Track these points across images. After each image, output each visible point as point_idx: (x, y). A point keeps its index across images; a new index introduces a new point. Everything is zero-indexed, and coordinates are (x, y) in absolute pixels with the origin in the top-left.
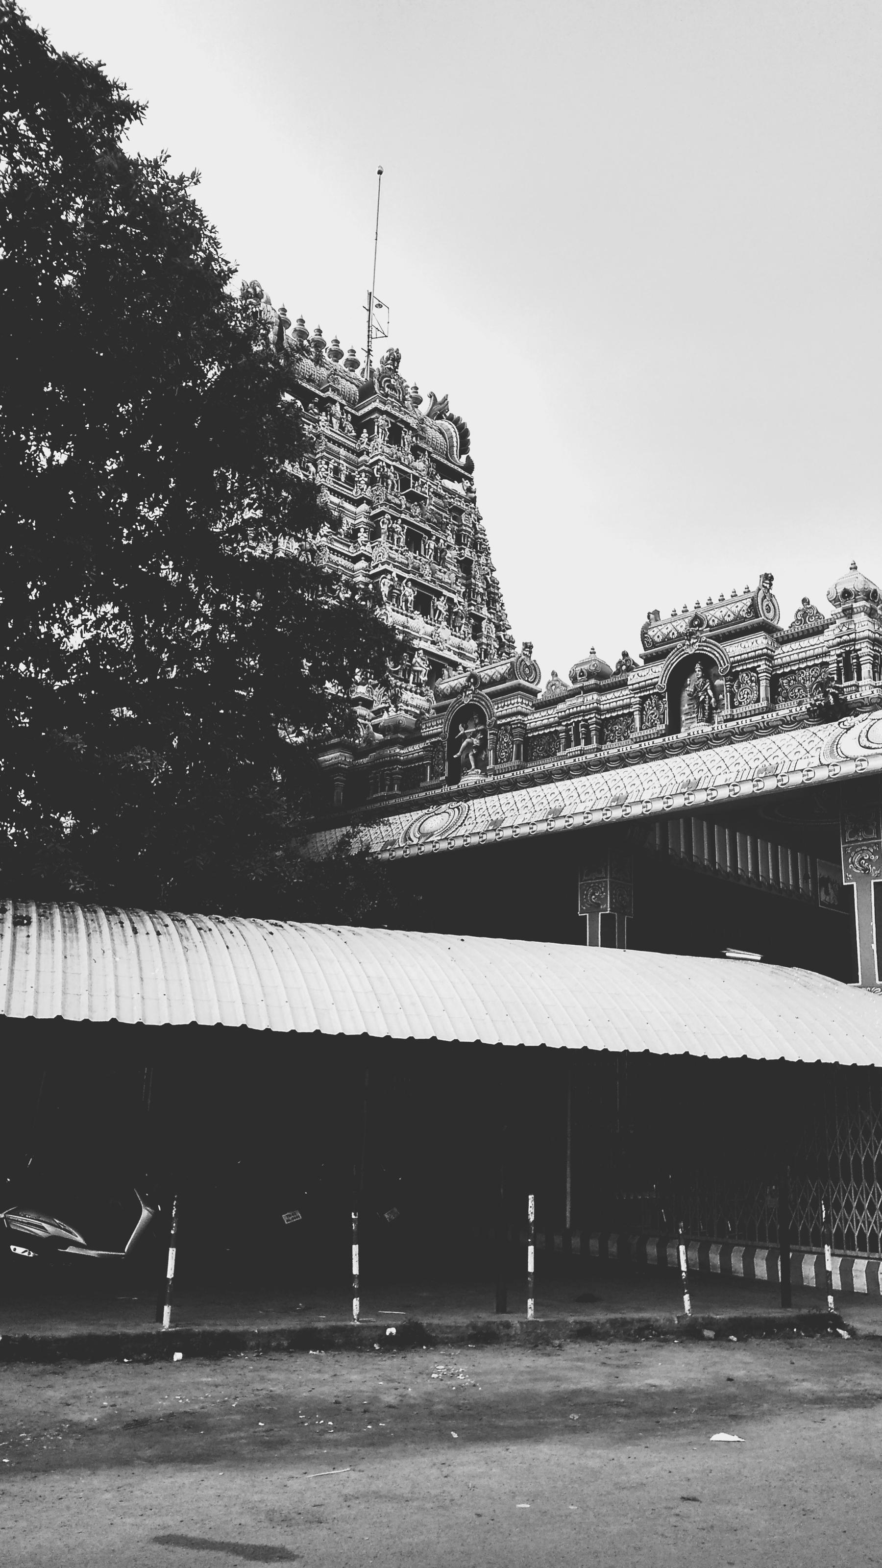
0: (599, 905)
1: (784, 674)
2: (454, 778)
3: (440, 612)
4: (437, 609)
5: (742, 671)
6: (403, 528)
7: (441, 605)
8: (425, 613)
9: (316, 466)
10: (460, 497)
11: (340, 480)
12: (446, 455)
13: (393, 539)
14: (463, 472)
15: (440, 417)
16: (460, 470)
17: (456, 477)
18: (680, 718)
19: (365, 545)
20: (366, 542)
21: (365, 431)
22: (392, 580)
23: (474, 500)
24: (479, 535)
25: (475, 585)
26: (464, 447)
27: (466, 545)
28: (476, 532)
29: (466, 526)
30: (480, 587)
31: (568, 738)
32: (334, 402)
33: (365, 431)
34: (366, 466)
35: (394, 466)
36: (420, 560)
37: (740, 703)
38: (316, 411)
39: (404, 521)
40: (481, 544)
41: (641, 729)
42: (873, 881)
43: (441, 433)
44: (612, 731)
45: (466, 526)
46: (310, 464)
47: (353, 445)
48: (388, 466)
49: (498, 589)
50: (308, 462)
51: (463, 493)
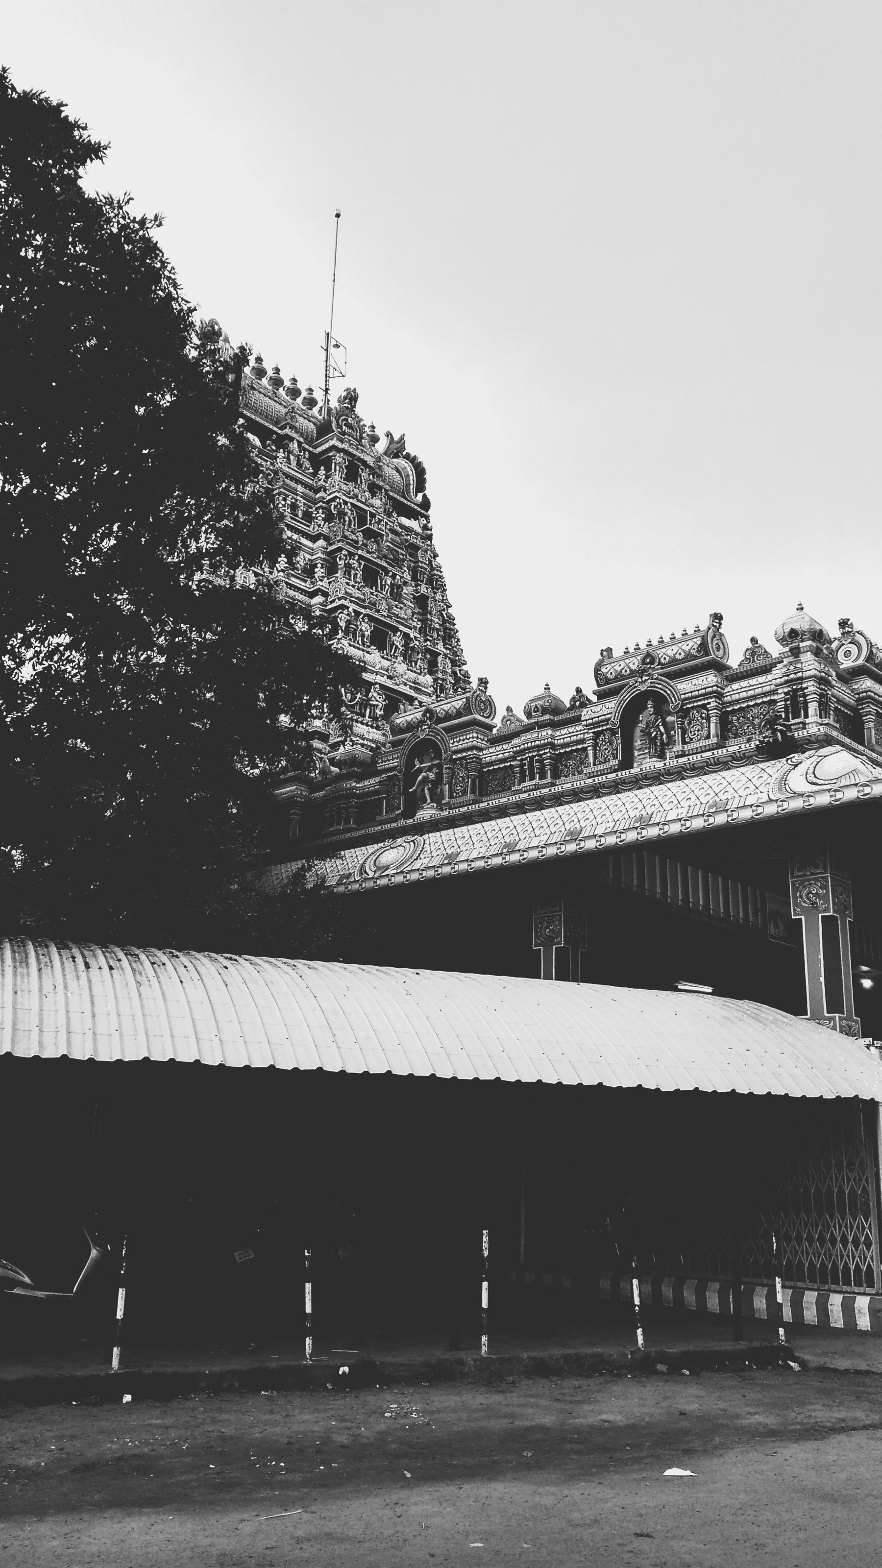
2: (410, 813)
3: (397, 647)
5: (693, 708)
6: (360, 564)
7: (398, 640)
8: (381, 648)
10: (417, 534)
11: (297, 515)
13: (350, 575)
15: (396, 456)
17: (412, 514)
18: (633, 754)
19: (322, 581)
21: (322, 468)
22: (348, 615)
23: (430, 538)
25: (432, 621)
27: (422, 581)
28: (432, 569)
29: (422, 562)
30: (436, 622)
31: (523, 772)
32: (292, 439)
33: (322, 468)
34: (324, 502)
37: (691, 739)
38: (274, 447)
39: (361, 557)
44: (566, 766)
45: (422, 562)
47: (311, 482)
48: (346, 503)
49: (454, 625)
51: (420, 530)
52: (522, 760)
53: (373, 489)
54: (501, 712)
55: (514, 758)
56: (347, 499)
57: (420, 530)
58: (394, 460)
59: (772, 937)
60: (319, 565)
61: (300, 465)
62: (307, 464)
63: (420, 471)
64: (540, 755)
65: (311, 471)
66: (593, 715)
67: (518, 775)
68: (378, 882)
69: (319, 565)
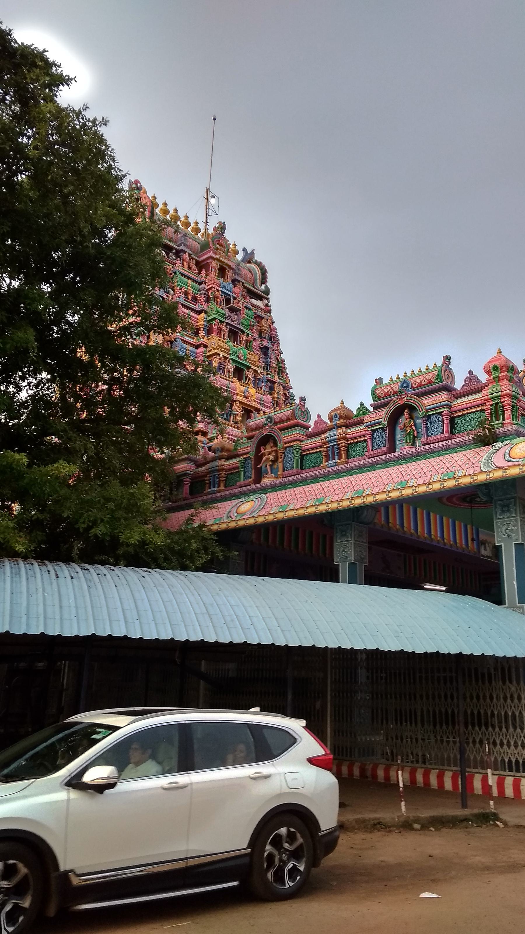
0: (347, 557)
1: (459, 416)
2: (258, 480)
3: (249, 378)
4: (247, 376)
5: (433, 414)
7: (250, 374)
9: (174, 290)
10: (261, 309)
13: (220, 335)
14: (263, 294)
15: (249, 262)
16: (261, 293)
19: (203, 338)
22: (220, 359)
23: (269, 311)
24: (273, 333)
25: (271, 362)
26: (264, 280)
27: (265, 338)
28: (271, 331)
29: (265, 327)
32: (185, 252)
34: (205, 291)
35: (221, 291)
36: (237, 347)
37: (432, 434)
38: (174, 257)
40: (274, 337)
41: (372, 450)
44: (354, 451)
45: (265, 327)
46: (170, 289)
48: (218, 291)
50: (169, 288)
51: (263, 307)
53: (234, 282)
57: (263, 307)
59: (483, 556)
60: (202, 329)
61: (189, 268)
62: (194, 267)
63: (264, 272)
65: (197, 271)
66: (371, 420)
67: (325, 457)
69: (202, 329)
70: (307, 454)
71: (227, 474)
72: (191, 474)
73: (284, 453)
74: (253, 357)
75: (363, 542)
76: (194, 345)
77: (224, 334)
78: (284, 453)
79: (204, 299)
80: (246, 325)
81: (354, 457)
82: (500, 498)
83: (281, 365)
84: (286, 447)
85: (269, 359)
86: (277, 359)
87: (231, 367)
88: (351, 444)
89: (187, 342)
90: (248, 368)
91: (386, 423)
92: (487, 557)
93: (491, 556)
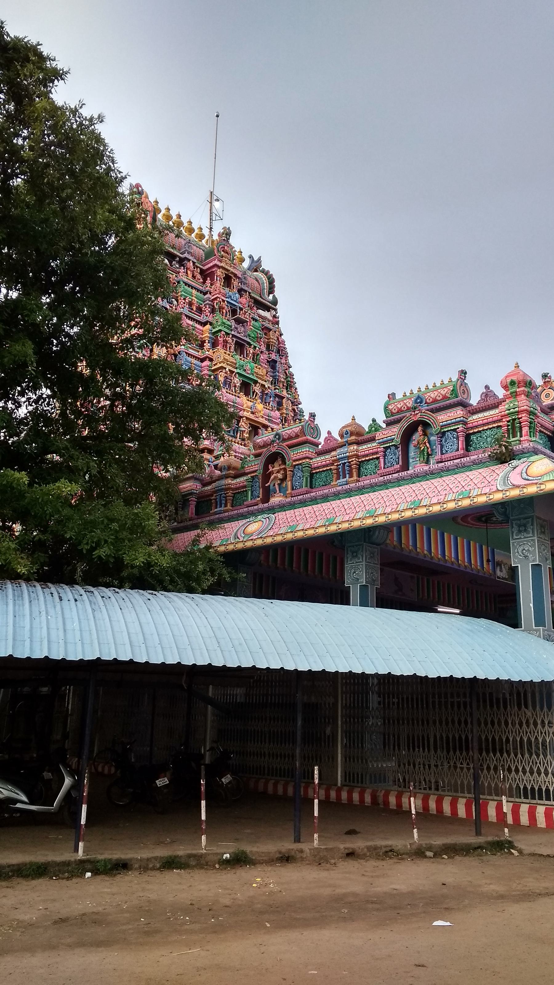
0: (358, 579)
2: (266, 499)
3: (257, 393)
4: (255, 391)
5: (448, 431)
7: (257, 389)
9: (177, 301)
10: (269, 321)
12: (260, 294)
14: (271, 305)
15: (256, 271)
16: (268, 304)
19: (209, 351)
20: (210, 349)
24: (281, 345)
26: (271, 290)
27: (273, 351)
29: (272, 339)
30: (282, 377)
33: (208, 279)
34: (210, 301)
35: (227, 301)
36: (244, 361)
37: (447, 451)
38: (177, 266)
39: (233, 336)
40: (282, 350)
41: (384, 468)
42: (530, 564)
43: (257, 280)
44: (366, 469)
45: (272, 339)
46: (173, 300)
50: (173, 298)
51: (271, 318)
52: (337, 465)
54: (324, 435)
55: (332, 464)
56: (225, 299)
57: (271, 318)
58: (254, 273)
59: (499, 578)
60: (207, 341)
61: (194, 277)
62: (199, 276)
64: (349, 462)
65: (201, 281)
67: (335, 475)
68: (237, 546)
69: (207, 341)
70: (316, 473)
71: (234, 494)
72: (196, 494)
73: (293, 471)
74: (260, 371)
75: (374, 563)
76: (199, 358)
77: (230, 347)
78: (293, 471)
79: (209, 309)
80: (253, 337)
81: (366, 476)
82: (516, 517)
83: (289, 379)
84: (295, 465)
85: (277, 374)
86: (285, 373)
87: (237, 381)
88: (362, 461)
89: (192, 355)
90: (256, 382)
91: (399, 440)
92: (503, 578)
93: (507, 577)
